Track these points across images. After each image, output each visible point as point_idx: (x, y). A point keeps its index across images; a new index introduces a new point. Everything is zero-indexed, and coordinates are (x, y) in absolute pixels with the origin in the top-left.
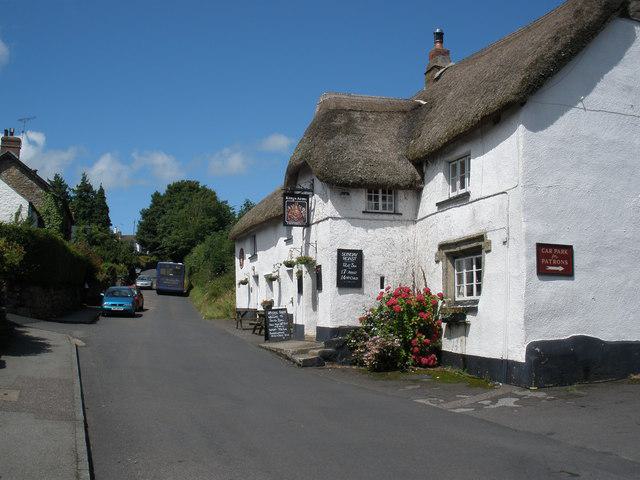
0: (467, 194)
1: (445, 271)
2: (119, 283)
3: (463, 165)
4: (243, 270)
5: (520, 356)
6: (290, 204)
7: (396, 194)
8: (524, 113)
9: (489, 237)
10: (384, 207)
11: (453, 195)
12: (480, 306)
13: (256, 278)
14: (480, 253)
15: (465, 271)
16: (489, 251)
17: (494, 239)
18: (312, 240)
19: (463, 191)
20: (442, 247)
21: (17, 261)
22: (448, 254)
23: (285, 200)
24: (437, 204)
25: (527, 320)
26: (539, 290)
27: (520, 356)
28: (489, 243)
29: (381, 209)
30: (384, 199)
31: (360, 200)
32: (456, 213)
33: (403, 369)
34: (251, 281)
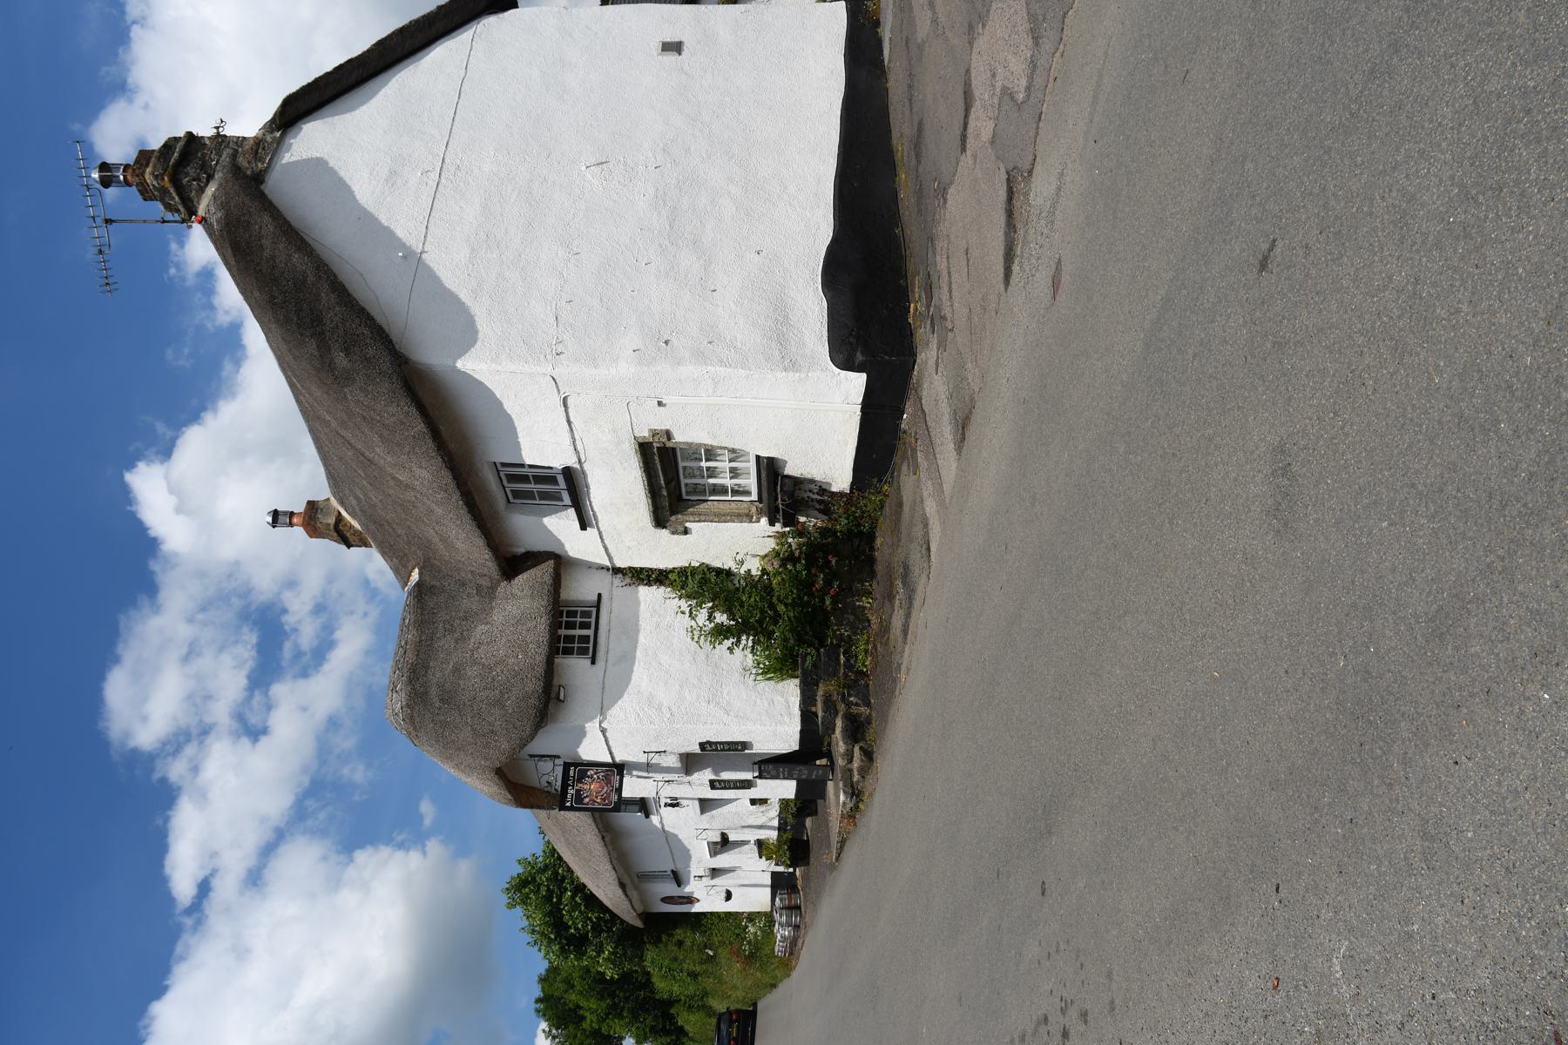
0: (567, 471)
1: (703, 518)
2: (813, 709)
3: (513, 478)
4: (708, 901)
5: (857, 382)
6: (579, 797)
7: (568, 603)
8: (429, 352)
9: (644, 433)
10: (585, 626)
11: (567, 500)
12: (764, 454)
13: (715, 872)
14: (674, 450)
15: (704, 464)
16: (668, 434)
17: (648, 422)
18: (643, 759)
19: (560, 479)
20: (660, 522)
21: (775, 837)
22: (673, 513)
23: (572, 809)
24: (583, 526)
25: (792, 366)
26: (739, 345)
27: (857, 382)
28: (654, 433)
29: (590, 632)
30: (571, 626)
31: (575, 668)
32: (599, 496)
33: (869, 720)
34: (723, 882)
